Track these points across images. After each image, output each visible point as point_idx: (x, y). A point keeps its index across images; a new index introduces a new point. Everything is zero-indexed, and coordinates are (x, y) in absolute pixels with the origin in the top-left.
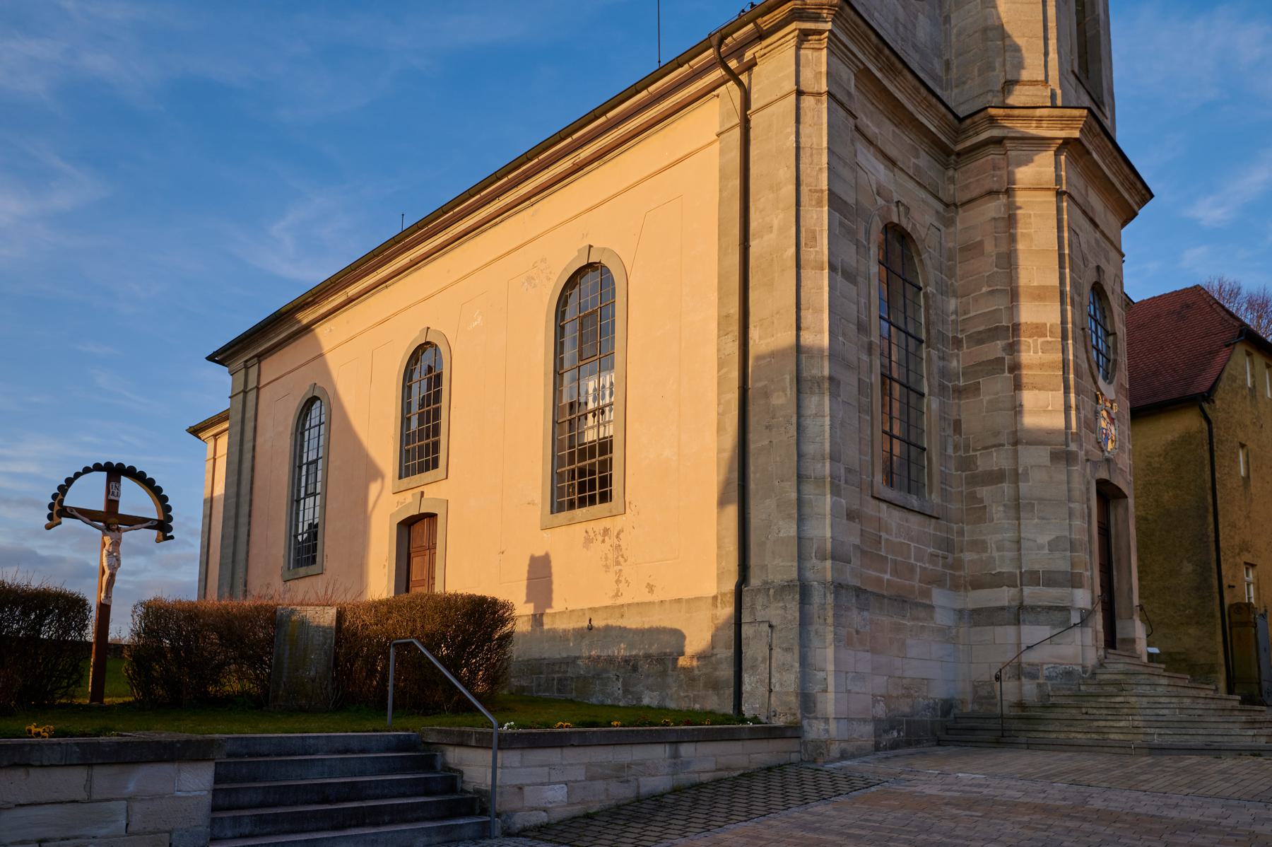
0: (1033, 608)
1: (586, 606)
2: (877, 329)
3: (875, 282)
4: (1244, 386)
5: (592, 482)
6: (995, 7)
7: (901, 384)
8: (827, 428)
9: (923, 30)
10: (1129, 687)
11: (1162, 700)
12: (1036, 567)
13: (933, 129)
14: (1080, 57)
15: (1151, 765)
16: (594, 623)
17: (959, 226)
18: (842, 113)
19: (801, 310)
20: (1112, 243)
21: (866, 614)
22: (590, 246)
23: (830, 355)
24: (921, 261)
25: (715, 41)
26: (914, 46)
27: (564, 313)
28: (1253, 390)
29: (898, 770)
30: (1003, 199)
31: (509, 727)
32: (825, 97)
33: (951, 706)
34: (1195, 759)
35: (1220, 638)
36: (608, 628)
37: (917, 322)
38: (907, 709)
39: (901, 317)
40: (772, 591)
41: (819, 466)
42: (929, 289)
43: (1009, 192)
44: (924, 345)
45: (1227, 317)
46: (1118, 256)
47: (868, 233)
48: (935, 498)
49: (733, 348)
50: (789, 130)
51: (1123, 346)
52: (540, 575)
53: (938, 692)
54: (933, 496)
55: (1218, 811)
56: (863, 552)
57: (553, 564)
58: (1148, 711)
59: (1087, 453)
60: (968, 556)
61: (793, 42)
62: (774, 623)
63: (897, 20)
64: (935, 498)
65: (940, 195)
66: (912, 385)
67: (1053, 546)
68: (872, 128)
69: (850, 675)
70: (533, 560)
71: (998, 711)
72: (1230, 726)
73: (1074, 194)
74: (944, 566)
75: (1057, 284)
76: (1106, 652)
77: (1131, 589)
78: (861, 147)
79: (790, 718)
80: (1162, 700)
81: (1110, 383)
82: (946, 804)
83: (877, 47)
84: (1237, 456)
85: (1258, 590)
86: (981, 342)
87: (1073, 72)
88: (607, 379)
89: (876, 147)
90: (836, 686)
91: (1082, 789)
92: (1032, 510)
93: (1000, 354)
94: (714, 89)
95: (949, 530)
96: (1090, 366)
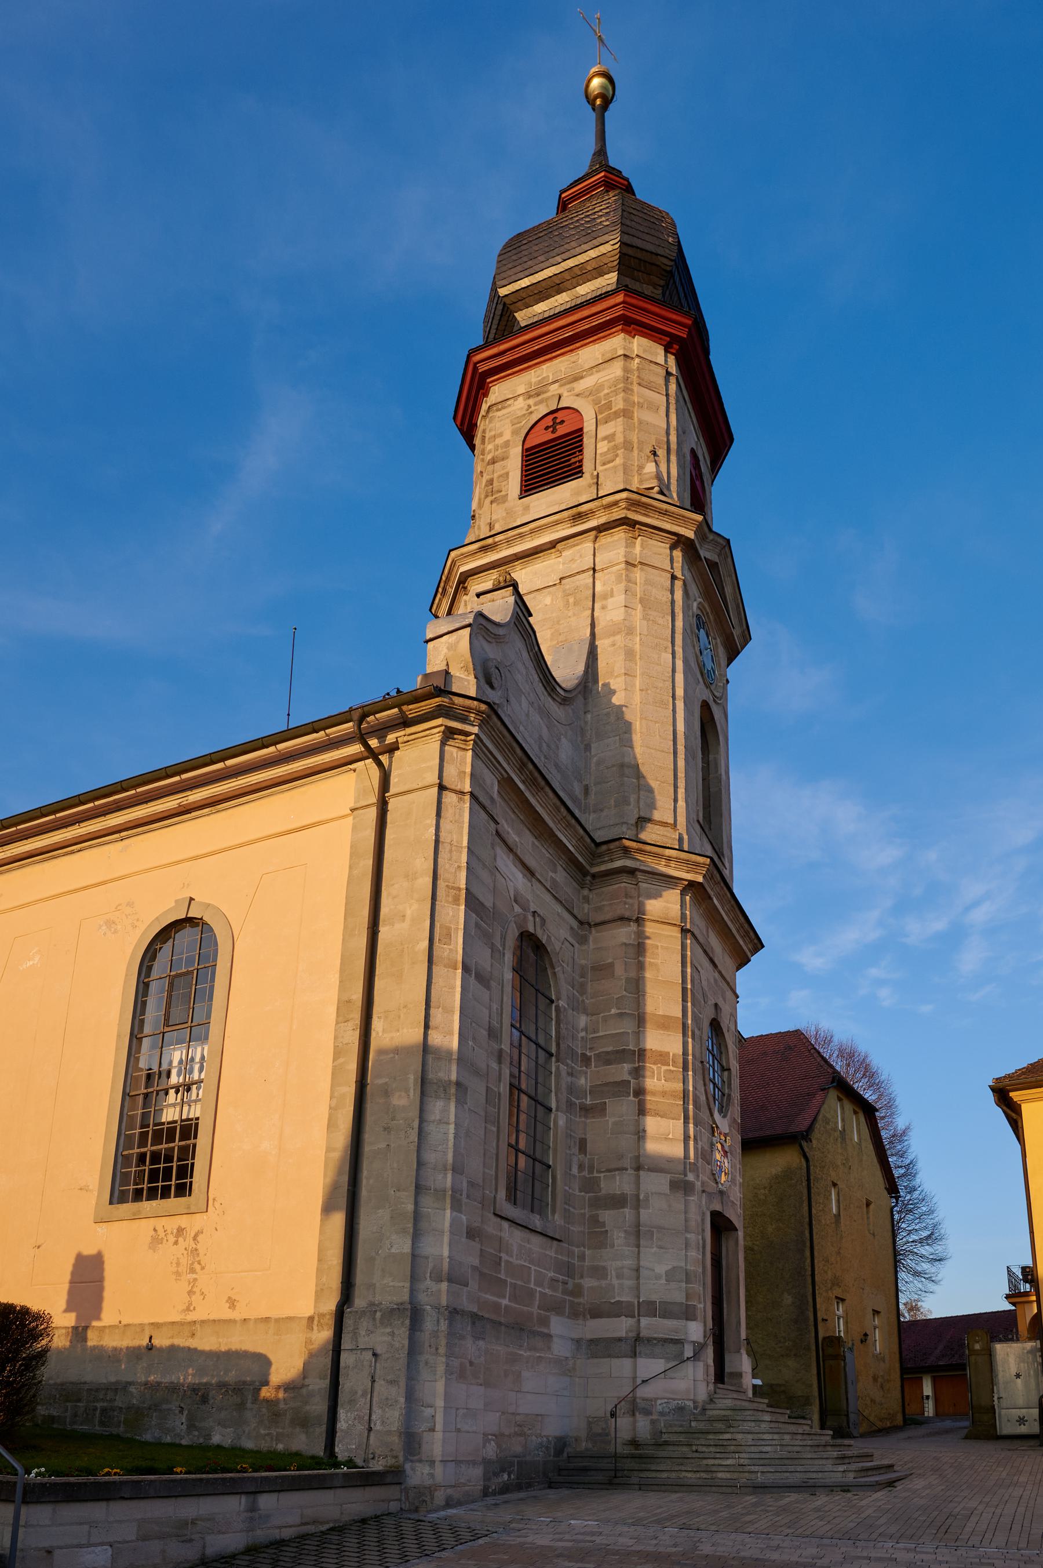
0: (649, 1340)
1: (146, 1321)
2: (508, 1036)
3: (508, 989)
4: (835, 1129)
5: (168, 1172)
6: (632, 747)
7: (530, 1097)
8: (451, 1137)
9: (566, 752)
10: (735, 1424)
11: (766, 1436)
12: (654, 1297)
13: (571, 848)
14: (704, 808)
15: (755, 1505)
16: (156, 1342)
17: (592, 946)
18: (483, 815)
19: (427, 1006)
20: (728, 984)
21: (481, 1343)
22: (191, 899)
23: (459, 1059)
24: (555, 974)
25: (356, 715)
26: (557, 766)
27: (150, 968)
28: (843, 1132)
29: (508, 1518)
30: (633, 927)
31: (38, 1474)
32: (467, 798)
33: (565, 1445)
34: (793, 1497)
35: (814, 1371)
36: (173, 1349)
37: (548, 1035)
38: (518, 1449)
39: (533, 1027)
40: (378, 1315)
41: (440, 1177)
42: (561, 1003)
43: (639, 921)
44: (554, 1059)
45: (822, 1063)
46: (734, 997)
47: (503, 938)
48: (558, 1219)
49: (353, 1037)
50: (428, 821)
51: (736, 1082)
52: (88, 1278)
53: (552, 1429)
54: (556, 1216)
55: (814, 1551)
56: (482, 1275)
57: (107, 1266)
58: (753, 1449)
59: (703, 1183)
60: (588, 1283)
61: (438, 737)
62: (379, 1351)
63: (541, 737)
64: (558, 1219)
65: (575, 912)
66: (540, 1098)
67: (670, 1276)
68: (513, 837)
69: (461, 1412)
70: (80, 1259)
71: (612, 1449)
72: (824, 1462)
73: (697, 932)
74: (564, 1292)
75: (680, 1015)
76: (715, 1388)
77: (739, 1323)
78: (501, 852)
79: (391, 1461)
80: (766, 1436)
81: (724, 1117)
82: (558, 1556)
83: (521, 760)
84: (831, 1194)
85: (846, 1323)
86: (608, 1062)
87: (698, 821)
88: (197, 1052)
89: (516, 855)
90: (445, 1423)
91: (692, 1533)
92: (652, 1238)
93: (627, 1077)
94: (351, 763)
95: (570, 1254)
96: (707, 1099)
